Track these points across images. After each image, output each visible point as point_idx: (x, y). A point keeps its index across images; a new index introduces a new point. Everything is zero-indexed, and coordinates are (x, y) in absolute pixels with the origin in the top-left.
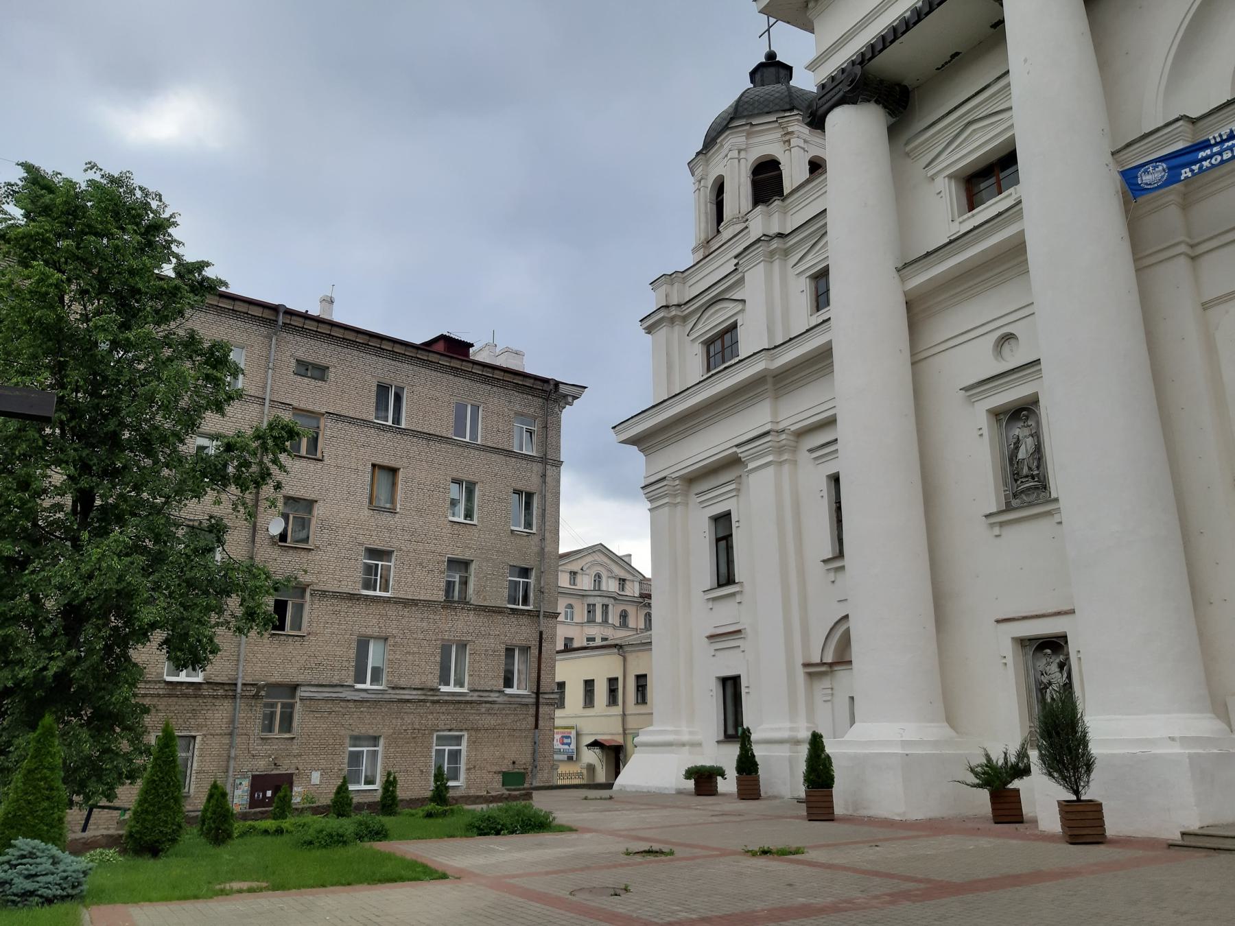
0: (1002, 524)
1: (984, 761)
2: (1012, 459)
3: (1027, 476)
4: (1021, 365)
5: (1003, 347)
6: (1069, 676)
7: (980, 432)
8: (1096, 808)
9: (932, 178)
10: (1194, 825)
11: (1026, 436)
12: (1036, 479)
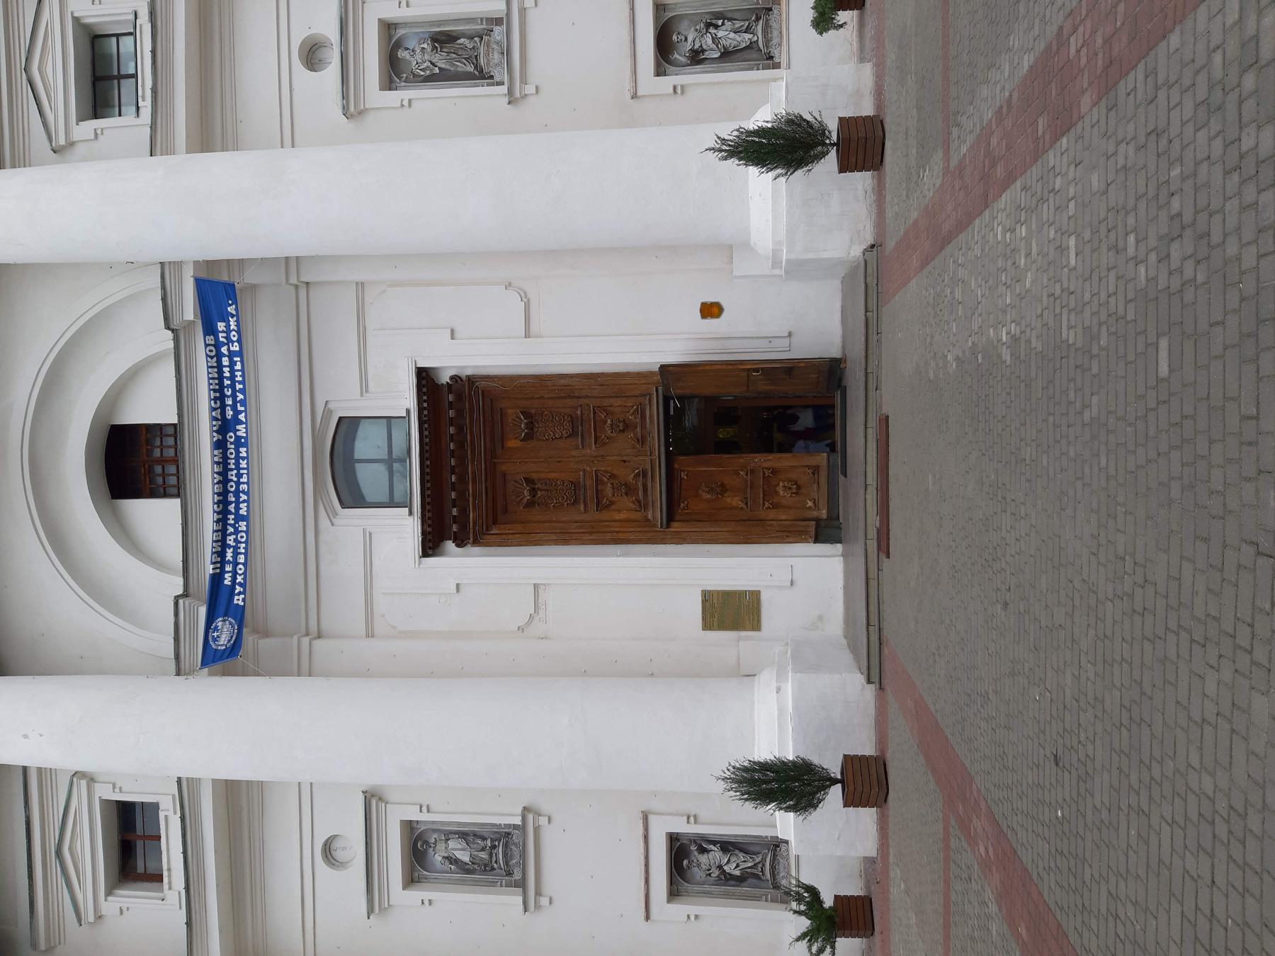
0: (538, 893)
1: (804, 943)
2: (467, 869)
3: (491, 855)
4: (365, 867)
5: (338, 859)
6: (714, 843)
7: (426, 902)
8: (851, 762)
9: (99, 917)
10: (860, 679)
11: (446, 848)
12: (497, 844)
